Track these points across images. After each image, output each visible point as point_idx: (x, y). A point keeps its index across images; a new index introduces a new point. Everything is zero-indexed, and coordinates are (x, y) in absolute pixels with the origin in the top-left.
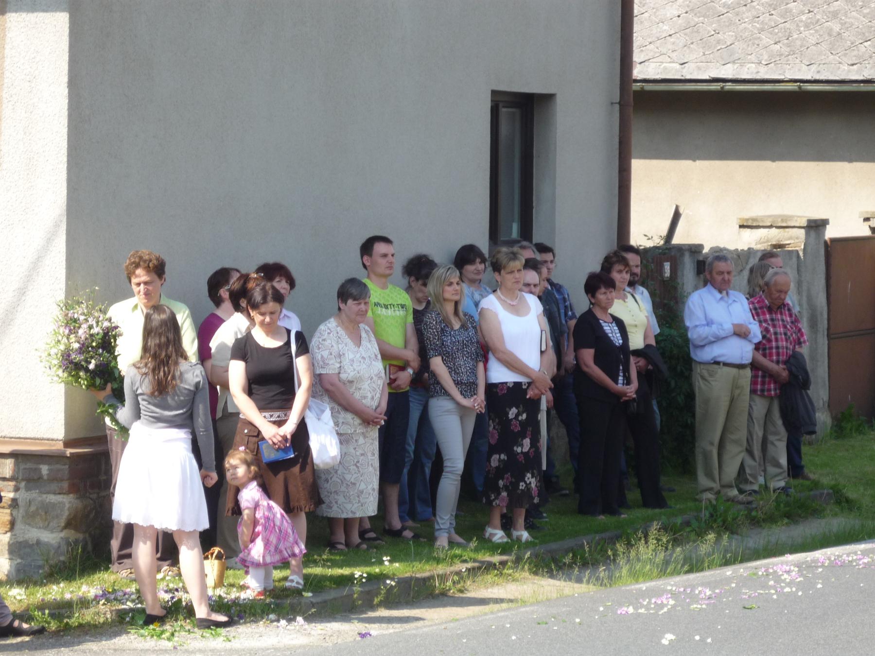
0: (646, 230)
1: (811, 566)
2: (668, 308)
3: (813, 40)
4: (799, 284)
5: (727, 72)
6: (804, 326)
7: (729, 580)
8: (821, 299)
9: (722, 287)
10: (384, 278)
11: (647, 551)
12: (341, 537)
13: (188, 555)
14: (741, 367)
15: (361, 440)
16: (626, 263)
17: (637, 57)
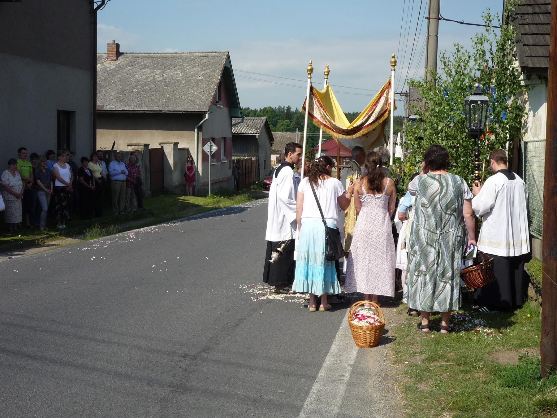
1: (139, 233)
3: (147, 101)
4: (142, 160)
8: (148, 163)
10: (24, 160)
11: (95, 230)
14: (123, 181)
15: (16, 202)
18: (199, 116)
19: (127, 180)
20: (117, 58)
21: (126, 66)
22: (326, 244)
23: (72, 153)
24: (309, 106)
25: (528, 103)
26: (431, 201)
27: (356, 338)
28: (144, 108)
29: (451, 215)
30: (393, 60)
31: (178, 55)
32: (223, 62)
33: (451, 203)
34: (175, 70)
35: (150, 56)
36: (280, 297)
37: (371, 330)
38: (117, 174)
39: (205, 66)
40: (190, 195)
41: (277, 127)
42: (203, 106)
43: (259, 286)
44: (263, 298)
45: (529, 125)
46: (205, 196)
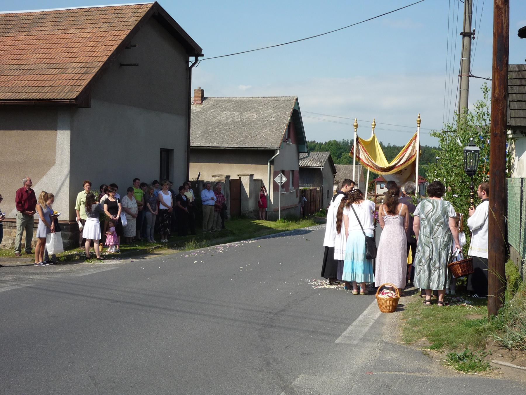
0: (193, 177)
2: (197, 193)
4: (224, 189)
5: (210, 145)
6: (225, 197)
7: (208, 250)
8: (229, 192)
9: (209, 189)
11: (192, 244)
12: (128, 241)
13: (96, 245)
14: (212, 206)
16: (188, 184)
17: (191, 141)
18: (272, 152)
19: (215, 205)
20: (202, 102)
21: (210, 109)
22: (366, 248)
23: (171, 183)
24: (356, 151)
25: (515, 151)
26: (427, 217)
27: (380, 306)
28: (224, 145)
29: (439, 226)
30: (419, 119)
31: (254, 99)
32: (292, 106)
33: (439, 218)
34: (251, 113)
35: (229, 100)
36: (333, 287)
37: (390, 301)
38: (208, 200)
39: (277, 109)
40: (263, 219)
41: (341, 159)
42: (275, 144)
43: (319, 280)
44: (321, 287)
45: (516, 166)
46: (276, 221)
